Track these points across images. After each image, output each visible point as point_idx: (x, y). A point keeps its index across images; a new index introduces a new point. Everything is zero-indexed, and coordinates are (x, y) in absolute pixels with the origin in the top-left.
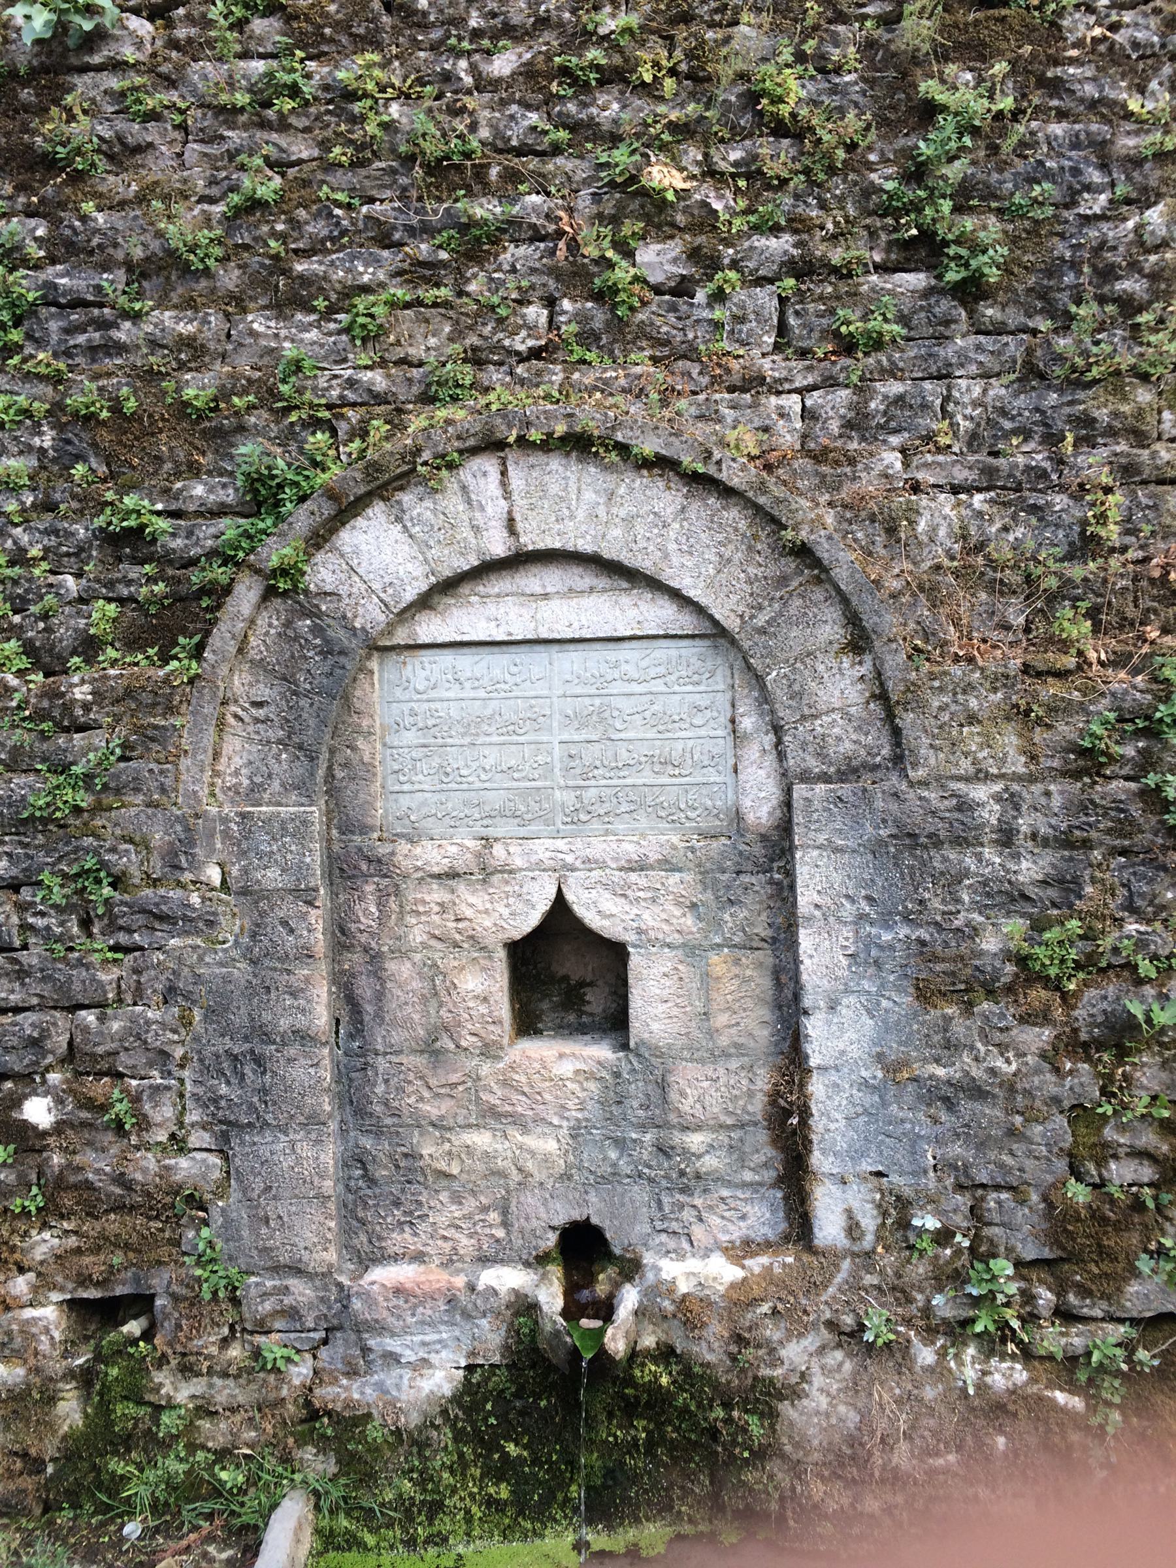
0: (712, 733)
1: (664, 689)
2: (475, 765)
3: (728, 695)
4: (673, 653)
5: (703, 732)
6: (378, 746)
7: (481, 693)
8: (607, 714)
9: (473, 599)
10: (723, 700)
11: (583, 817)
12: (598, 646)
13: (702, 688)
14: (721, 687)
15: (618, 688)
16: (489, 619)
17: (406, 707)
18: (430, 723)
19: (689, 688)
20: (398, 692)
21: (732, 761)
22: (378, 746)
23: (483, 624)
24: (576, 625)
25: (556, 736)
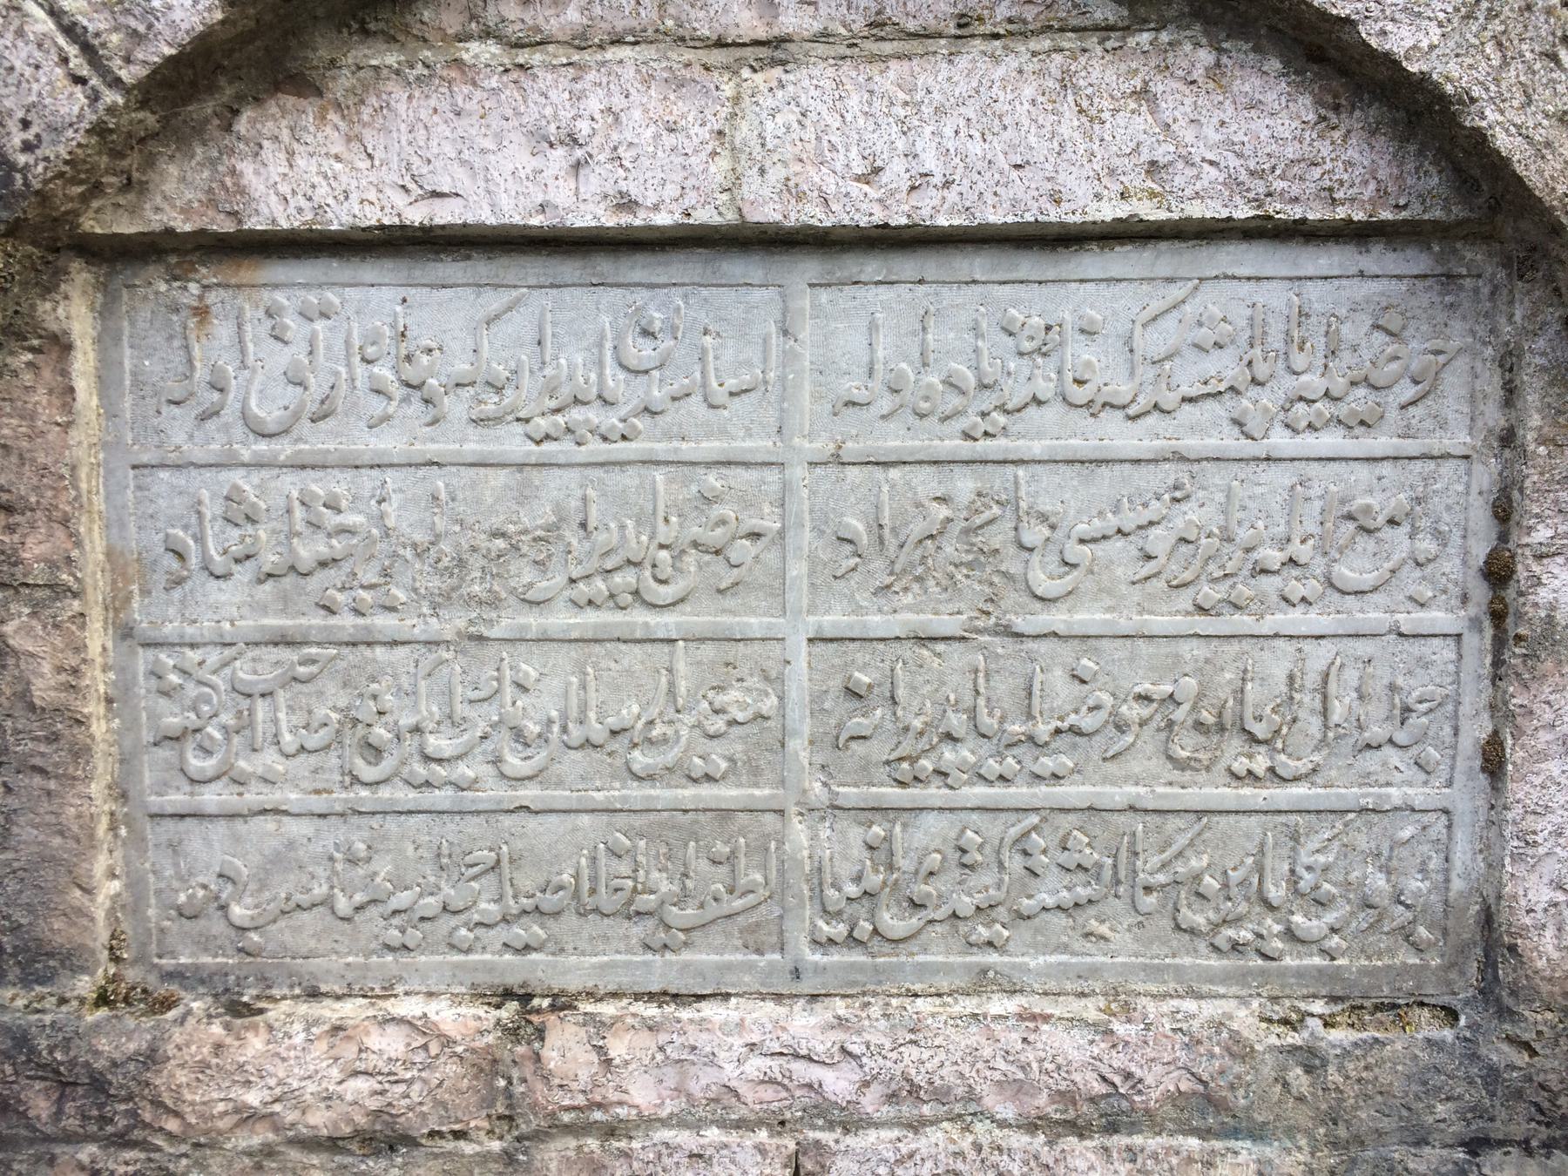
0: (1409, 620)
1: (1231, 442)
2: (481, 718)
3: (1485, 475)
4: (1276, 297)
5: (1372, 615)
6: (97, 638)
7: (512, 442)
8: (998, 537)
9: (479, 52)
10: (1462, 496)
11: (893, 921)
12: (976, 264)
13: (1381, 443)
14: (1458, 439)
15: (1047, 432)
16: (542, 140)
17: (209, 489)
18: (308, 551)
19: (1331, 441)
20: (179, 429)
21: (1477, 729)
22: (97, 638)
23: (517, 156)
24: (896, 173)
25: (799, 618)
